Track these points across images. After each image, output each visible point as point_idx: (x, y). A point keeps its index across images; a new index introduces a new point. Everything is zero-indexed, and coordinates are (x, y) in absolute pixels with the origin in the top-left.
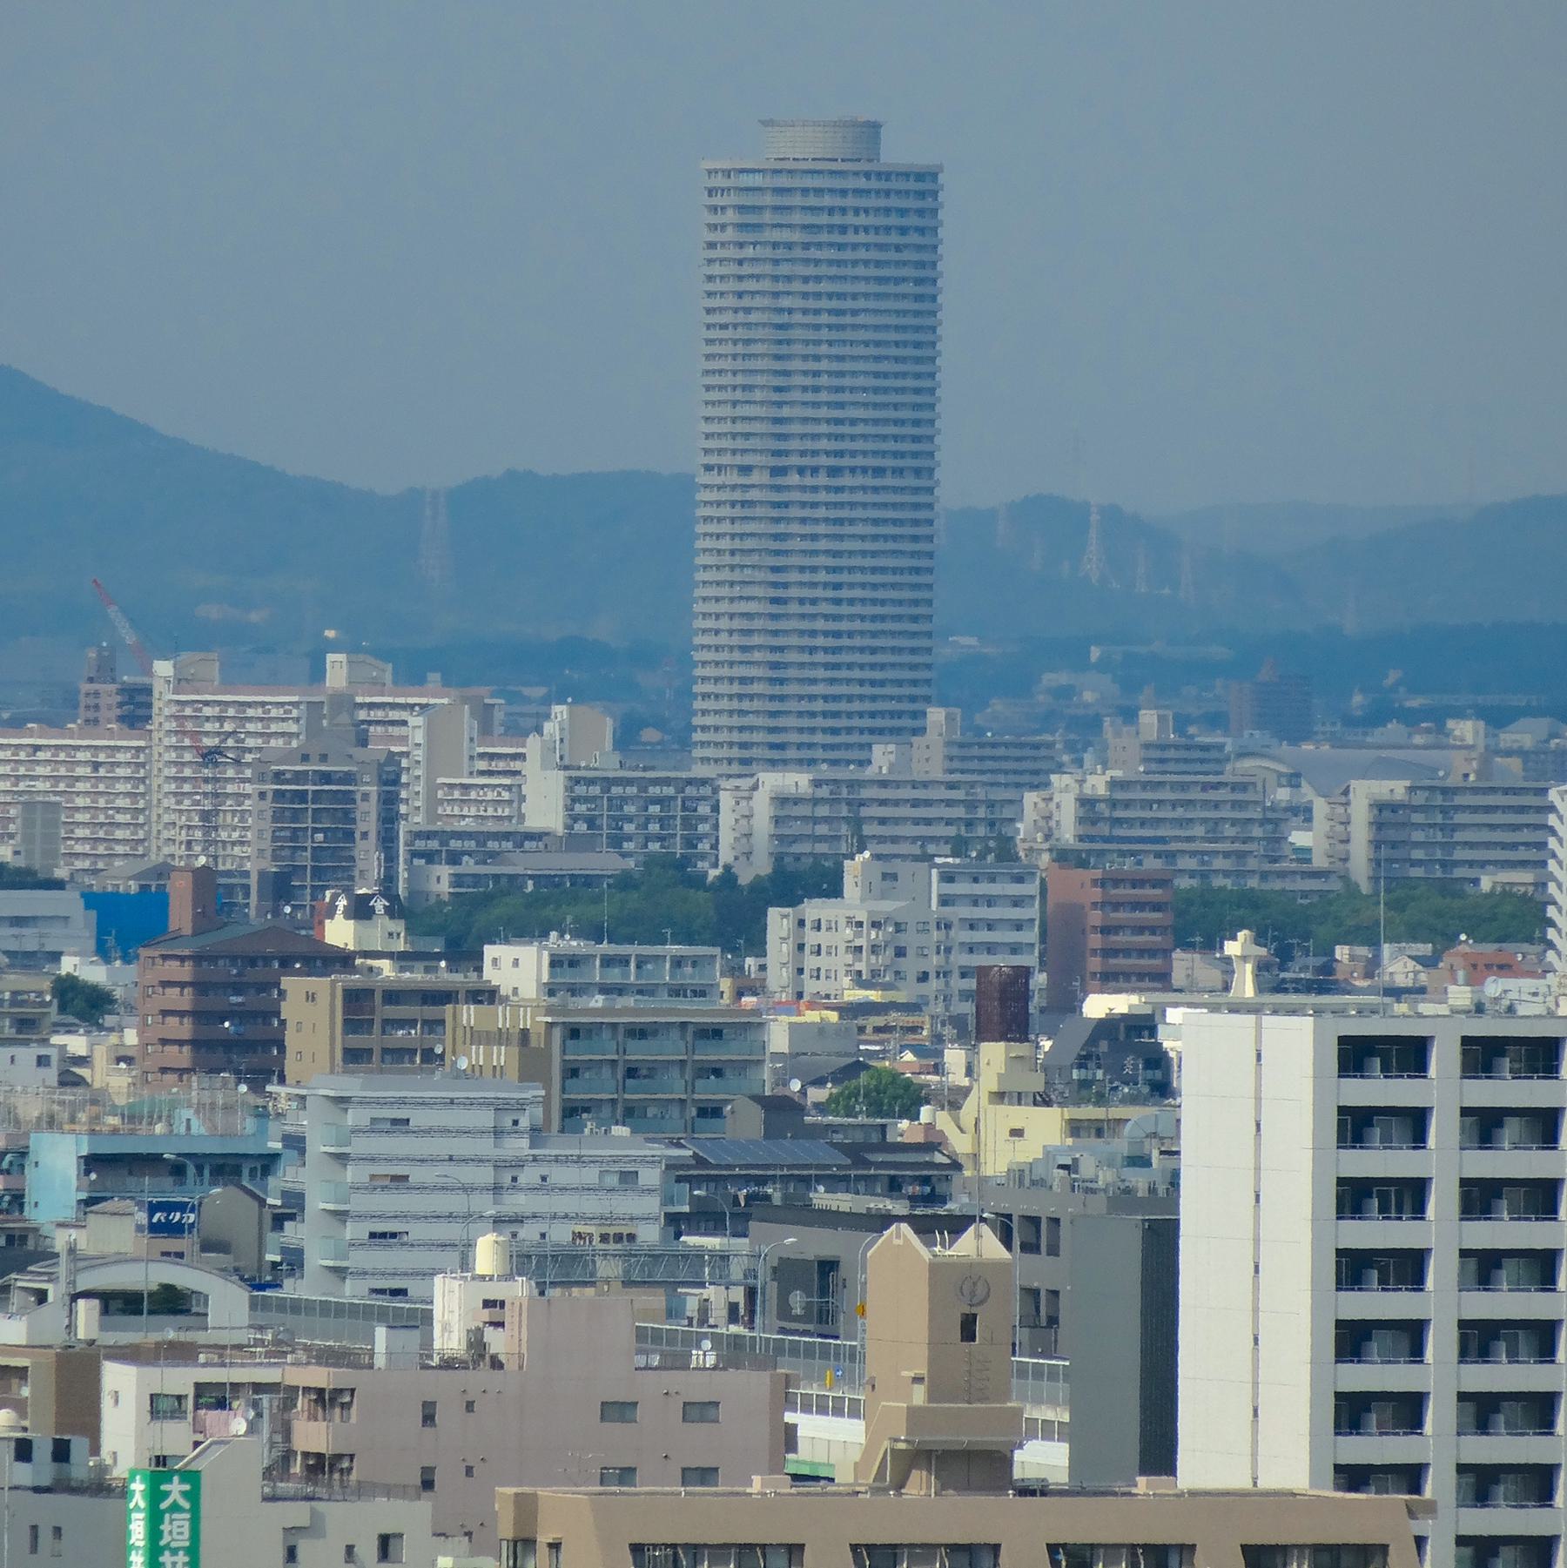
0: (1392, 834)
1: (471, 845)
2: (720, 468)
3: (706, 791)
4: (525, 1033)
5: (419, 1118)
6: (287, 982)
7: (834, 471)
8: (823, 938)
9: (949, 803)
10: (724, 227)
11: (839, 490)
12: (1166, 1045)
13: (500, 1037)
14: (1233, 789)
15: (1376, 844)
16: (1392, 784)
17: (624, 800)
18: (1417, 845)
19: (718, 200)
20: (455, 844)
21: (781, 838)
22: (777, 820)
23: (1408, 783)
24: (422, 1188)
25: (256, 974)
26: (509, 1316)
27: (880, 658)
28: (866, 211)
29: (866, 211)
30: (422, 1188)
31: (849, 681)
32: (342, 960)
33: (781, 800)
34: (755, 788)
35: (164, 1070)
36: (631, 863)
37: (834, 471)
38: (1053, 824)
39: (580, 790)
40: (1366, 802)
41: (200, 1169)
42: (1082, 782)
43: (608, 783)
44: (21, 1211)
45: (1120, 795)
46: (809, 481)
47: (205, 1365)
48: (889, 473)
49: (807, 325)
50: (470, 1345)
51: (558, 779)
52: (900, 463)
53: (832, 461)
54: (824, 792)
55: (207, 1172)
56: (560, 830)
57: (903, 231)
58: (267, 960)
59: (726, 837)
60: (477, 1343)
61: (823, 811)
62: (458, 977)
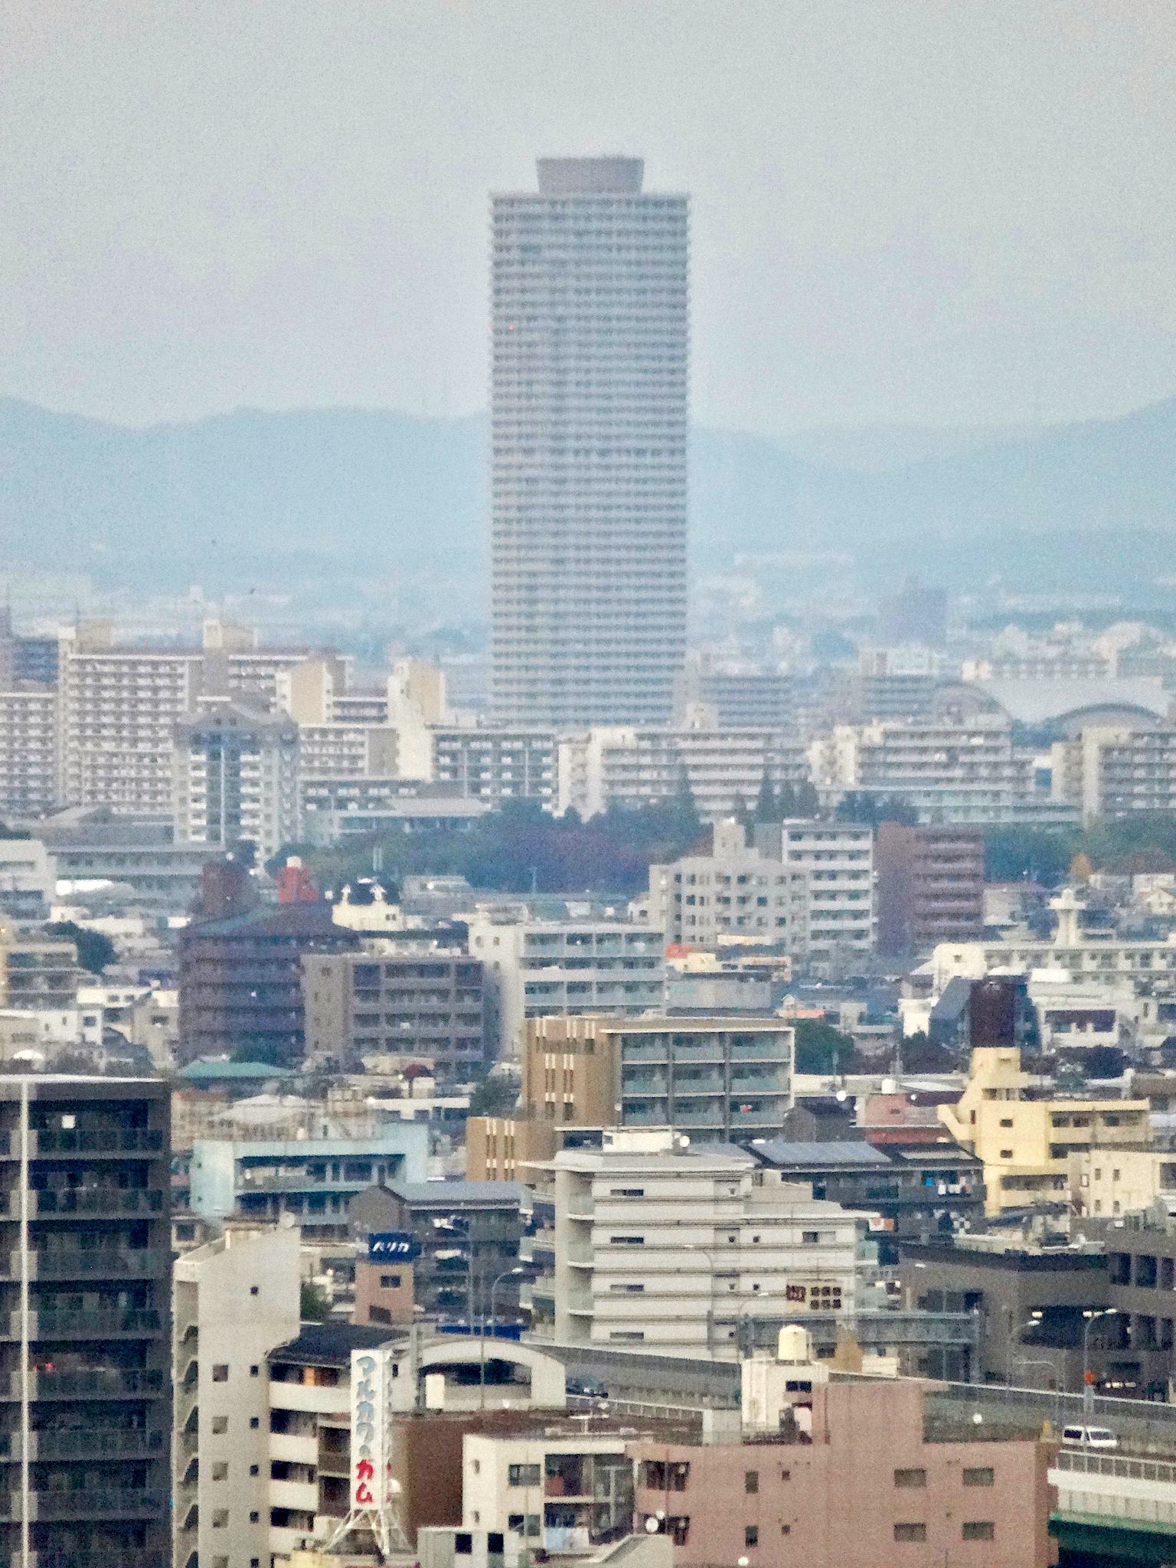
0: (1119, 772)
1: (355, 792)
3: (549, 745)
4: (591, 1043)
5: (651, 1188)
6: (307, 959)
7: (603, 453)
8: (697, 890)
11: (607, 467)
12: (1035, 1000)
13: (571, 1046)
15: (1107, 780)
16: (1116, 730)
17: (482, 753)
20: (342, 792)
23: (1130, 730)
24: (653, 1248)
25: (281, 951)
26: (814, 1397)
30: (653, 1248)
31: (617, 628)
32: (352, 939)
33: (610, 752)
34: (588, 740)
35: (201, 1033)
36: (488, 806)
37: (603, 453)
38: (836, 768)
39: (445, 745)
40: (1095, 746)
41: (335, 1168)
42: (860, 734)
43: (468, 739)
44: (187, 1204)
45: (891, 743)
50: (782, 1423)
51: (426, 739)
55: (342, 1172)
56: (430, 780)
58: (287, 939)
59: (565, 782)
60: (789, 1422)
62: (444, 953)
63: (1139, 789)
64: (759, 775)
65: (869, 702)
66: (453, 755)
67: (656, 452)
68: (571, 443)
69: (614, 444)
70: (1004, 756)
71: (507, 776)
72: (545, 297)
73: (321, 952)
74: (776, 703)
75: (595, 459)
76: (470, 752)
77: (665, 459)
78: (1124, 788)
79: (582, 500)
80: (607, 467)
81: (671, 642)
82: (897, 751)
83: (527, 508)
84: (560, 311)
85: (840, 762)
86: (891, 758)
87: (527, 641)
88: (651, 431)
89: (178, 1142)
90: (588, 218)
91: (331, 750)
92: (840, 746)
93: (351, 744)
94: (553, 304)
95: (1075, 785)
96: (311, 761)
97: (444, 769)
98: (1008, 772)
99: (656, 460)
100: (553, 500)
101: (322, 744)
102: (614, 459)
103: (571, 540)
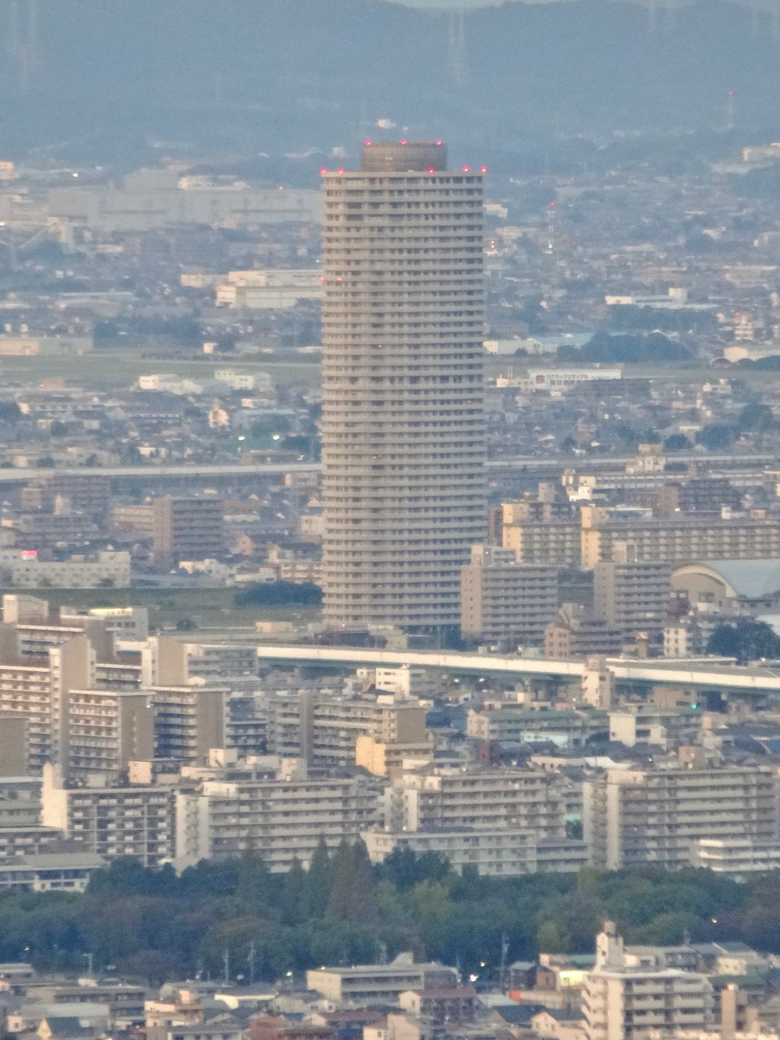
0: (634, 807)
2: (337, 378)
7: (414, 380)
9: (331, 800)
10: (337, 217)
11: (417, 392)
14: (526, 782)
15: (625, 814)
17: (108, 808)
18: (652, 814)
19: (332, 199)
21: (217, 828)
22: (215, 816)
27: (447, 503)
28: (433, 204)
29: (433, 204)
37: (414, 380)
38: (403, 810)
39: (78, 803)
40: (616, 787)
45: (448, 790)
46: (397, 386)
47: (77, 874)
48: (451, 379)
49: (394, 282)
52: (458, 372)
53: (413, 373)
54: (245, 796)
57: (458, 216)
61: (245, 809)
63: (652, 820)
64: (314, 843)
65: (619, 586)
66: (84, 809)
67: (458, 378)
70: (540, 798)
71: (129, 826)
72: (367, 255)
74: (543, 588)
75: (407, 385)
76: (99, 808)
78: (640, 821)
79: (396, 418)
80: (417, 392)
82: (452, 796)
83: (354, 424)
84: (378, 267)
85: (406, 805)
86: (448, 802)
87: (354, 531)
88: (453, 361)
89: (252, 767)
90: (401, 192)
91: (92, 713)
92: (407, 792)
93: (108, 708)
94: (372, 262)
95: (601, 816)
96: (77, 721)
97: (78, 822)
98: (543, 810)
99: (458, 385)
100: (373, 419)
101: (85, 707)
102: (422, 385)
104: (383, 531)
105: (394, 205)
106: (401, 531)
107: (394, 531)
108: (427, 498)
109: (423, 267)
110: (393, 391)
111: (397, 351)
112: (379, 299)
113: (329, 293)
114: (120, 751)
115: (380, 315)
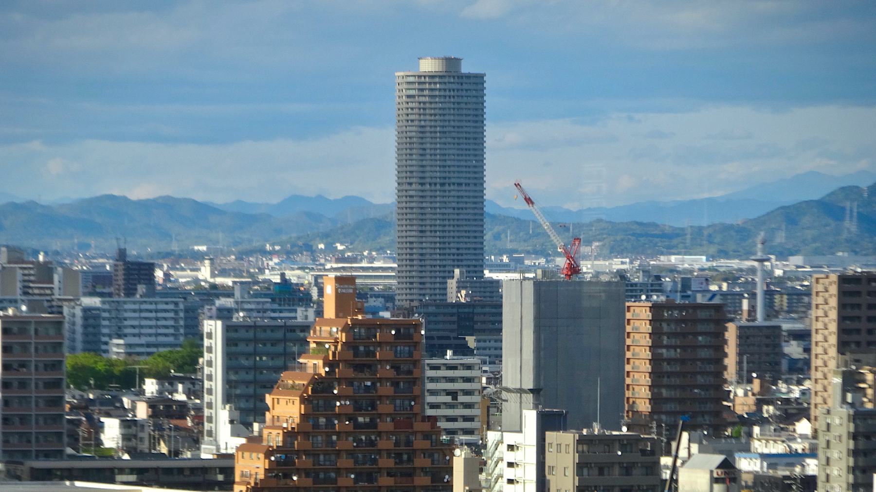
37: (442, 184)
46: (433, 187)
52: (467, 181)
67: (467, 185)
68: (428, 180)
69: (447, 181)
73: (243, 227)
77: (472, 188)
81: (475, 266)
94: (420, 121)
99: (467, 188)
103: (428, 216)
104: (425, 266)
105: (432, 90)
106: (435, 266)
107: (431, 266)
108: (449, 237)
109: (449, 163)
110: (431, 191)
111: (433, 169)
112: (424, 140)
113: (399, 254)
114: (315, 362)
115: (424, 149)
